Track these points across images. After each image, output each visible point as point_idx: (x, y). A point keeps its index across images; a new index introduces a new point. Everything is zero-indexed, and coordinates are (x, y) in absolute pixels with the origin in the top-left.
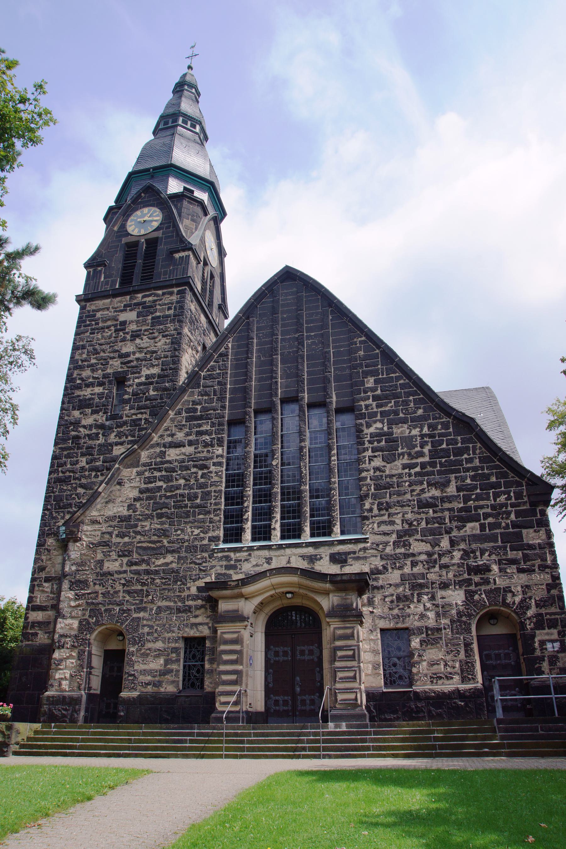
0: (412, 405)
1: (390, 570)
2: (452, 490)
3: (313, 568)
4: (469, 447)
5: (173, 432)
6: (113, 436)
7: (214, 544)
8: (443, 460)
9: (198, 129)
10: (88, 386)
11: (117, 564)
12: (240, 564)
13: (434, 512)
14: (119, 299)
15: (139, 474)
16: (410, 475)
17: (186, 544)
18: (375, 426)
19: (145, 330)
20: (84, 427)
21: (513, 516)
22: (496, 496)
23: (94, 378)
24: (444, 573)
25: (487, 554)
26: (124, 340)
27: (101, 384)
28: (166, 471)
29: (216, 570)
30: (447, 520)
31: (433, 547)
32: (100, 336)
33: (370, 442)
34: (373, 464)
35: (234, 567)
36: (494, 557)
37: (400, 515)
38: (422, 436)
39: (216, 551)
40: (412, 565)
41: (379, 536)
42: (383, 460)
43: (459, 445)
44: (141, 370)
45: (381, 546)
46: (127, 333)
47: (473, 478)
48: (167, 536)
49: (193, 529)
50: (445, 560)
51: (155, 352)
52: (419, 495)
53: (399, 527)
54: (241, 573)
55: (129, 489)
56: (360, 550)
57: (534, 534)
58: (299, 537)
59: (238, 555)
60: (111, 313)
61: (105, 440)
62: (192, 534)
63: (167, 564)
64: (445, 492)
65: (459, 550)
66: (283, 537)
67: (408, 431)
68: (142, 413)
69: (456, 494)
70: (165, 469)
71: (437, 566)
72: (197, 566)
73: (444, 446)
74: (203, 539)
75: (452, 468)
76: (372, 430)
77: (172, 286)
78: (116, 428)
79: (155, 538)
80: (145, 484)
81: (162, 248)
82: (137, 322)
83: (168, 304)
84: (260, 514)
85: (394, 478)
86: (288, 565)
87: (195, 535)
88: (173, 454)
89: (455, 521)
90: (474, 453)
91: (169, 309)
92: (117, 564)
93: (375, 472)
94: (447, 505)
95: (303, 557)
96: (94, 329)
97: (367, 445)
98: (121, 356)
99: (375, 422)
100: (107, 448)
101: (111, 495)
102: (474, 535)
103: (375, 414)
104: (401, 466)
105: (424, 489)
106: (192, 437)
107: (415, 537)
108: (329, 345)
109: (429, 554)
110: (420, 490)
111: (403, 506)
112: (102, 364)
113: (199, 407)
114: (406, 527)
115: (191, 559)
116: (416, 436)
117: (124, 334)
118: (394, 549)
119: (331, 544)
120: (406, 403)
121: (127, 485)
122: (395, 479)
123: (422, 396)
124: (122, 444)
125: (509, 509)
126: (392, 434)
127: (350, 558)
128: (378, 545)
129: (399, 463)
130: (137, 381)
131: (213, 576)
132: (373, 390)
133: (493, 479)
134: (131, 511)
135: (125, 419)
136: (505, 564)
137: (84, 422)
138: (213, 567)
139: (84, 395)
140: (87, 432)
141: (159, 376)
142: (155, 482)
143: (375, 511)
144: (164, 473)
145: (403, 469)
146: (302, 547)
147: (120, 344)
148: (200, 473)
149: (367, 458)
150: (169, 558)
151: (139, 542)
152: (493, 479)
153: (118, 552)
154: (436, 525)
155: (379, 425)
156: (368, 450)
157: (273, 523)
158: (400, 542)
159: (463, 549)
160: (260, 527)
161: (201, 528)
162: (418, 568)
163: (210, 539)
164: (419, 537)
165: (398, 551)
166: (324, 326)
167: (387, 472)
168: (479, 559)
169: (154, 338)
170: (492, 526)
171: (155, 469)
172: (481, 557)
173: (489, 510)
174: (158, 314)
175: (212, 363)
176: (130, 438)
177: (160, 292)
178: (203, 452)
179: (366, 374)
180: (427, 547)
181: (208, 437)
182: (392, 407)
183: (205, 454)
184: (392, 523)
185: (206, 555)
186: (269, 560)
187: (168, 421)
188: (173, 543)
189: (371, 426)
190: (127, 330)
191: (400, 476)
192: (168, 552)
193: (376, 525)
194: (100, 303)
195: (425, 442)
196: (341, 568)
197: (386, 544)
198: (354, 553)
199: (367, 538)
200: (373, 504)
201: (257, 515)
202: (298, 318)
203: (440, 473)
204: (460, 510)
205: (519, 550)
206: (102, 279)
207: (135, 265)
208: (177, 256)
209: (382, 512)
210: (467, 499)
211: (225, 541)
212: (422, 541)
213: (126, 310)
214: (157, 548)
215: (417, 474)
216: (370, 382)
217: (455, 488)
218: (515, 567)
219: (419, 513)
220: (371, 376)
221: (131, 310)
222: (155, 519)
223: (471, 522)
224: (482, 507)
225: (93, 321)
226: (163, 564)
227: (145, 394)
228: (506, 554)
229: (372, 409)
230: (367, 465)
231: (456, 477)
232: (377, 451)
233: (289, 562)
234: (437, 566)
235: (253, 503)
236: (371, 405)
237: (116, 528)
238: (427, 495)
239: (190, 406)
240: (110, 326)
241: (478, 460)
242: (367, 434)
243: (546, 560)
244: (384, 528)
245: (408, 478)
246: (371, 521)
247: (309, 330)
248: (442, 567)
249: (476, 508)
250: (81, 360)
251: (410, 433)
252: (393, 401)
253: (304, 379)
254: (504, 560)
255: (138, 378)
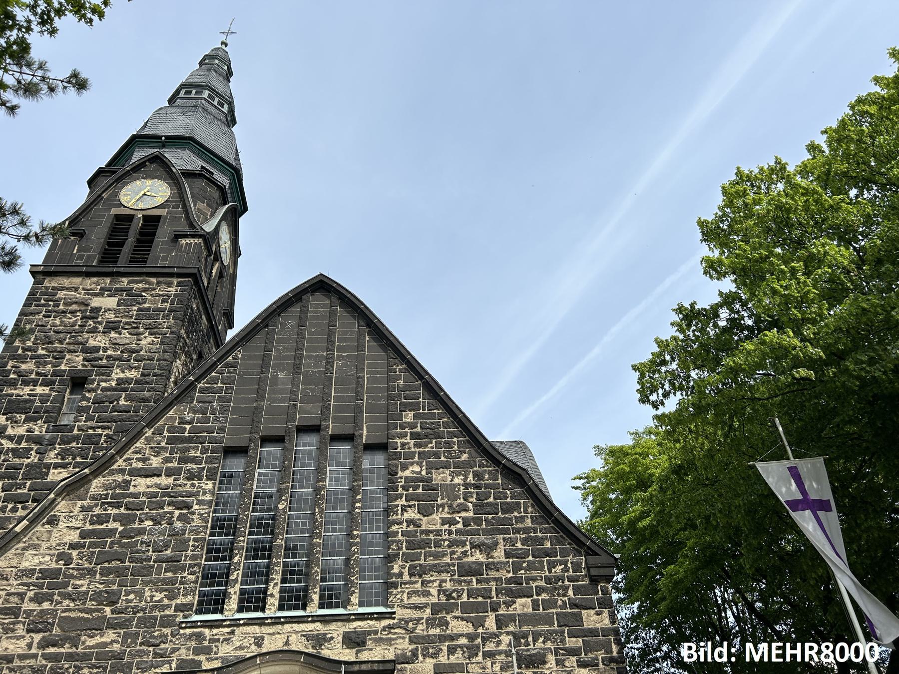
0: (456, 447)
1: (421, 658)
2: (499, 554)
3: (320, 653)
4: (520, 503)
5: (147, 456)
6: (52, 454)
7: (182, 614)
8: (490, 516)
9: (225, 109)
10: (26, 383)
11: (23, 643)
12: (216, 646)
13: (478, 581)
14: (95, 279)
15: (83, 509)
16: (450, 533)
17: (140, 614)
18: (411, 469)
19: (127, 323)
20: (10, 438)
21: (570, 592)
22: (551, 565)
23: (38, 374)
24: (489, 664)
25: (541, 640)
26: (94, 331)
27: (45, 384)
28: (127, 509)
29: (180, 655)
30: (494, 593)
31: (476, 627)
32: (57, 322)
33: (405, 488)
34: (406, 515)
35: (207, 651)
36: (549, 645)
37: (436, 584)
38: (466, 486)
39: (184, 625)
40: (448, 651)
41: (408, 611)
42: (418, 512)
43: (509, 500)
44: (112, 371)
45: (410, 625)
46: (100, 323)
47: (524, 542)
48: (112, 603)
49: (155, 593)
50: (490, 646)
51: (138, 351)
52: (459, 558)
53: (435, 600)
54: (216, 659)
55: (65, 531)
56: (384, 629)
57: (595, 617)
58: (304, 608)
59: (215, 631)
60: (80, 296)
61: (39, 460)
62: (151, 599)
63: (105, 645)
64: (492, 557)
65: (508, 633)
66: (281, 608)
67: (450, 478)
68: (103, 428)
69: (505, 560)
70: (126, 505)
71: (480, 654)
72: (151, 649)
73: (491, 500)
74: (169, 606)
75: (501, 527)
76: (407, 473)
77: (172, 275)
78: (59, 444)
79: (89, 604)
80: (92, 523)
81: (164, 232)
82: (116, 312)
83: (163, 295)
84: (253, 574)
85: (431, 535)
86: (285, 648)
87: (156, 601)
88: (141, 485)
89: (502, 594)
90: (526, 511)
91: (163, 301)
92: (23, 643)
93: (408, 526)
94: (493, 574)
95: (308, 637)
96: (50, 311)
97: (400, 491)
98: (86, 350)
99: (412, 464)
100: (39, 471)
101: (34, 538)
102: (525, 615)
103: (411, 455)
104: (439, 521)
105: (467, 551)
106: (174, 465)
107: (454, 614)
108: (364, 369)
109: (471, 637)
110: (462, 552)
111: (440, 572)
112: (54, 358)
113: (188, 427)
114: (443, 599)
115: (144, 637)
116: (459, 484)
117: (94, 323)
118: (427, 628)
119: (346, 619)
120: (449, 444)
121: (62, 525)
122: (431, 536)
123: (467, 438)
124: (64, 466)
125: (567, 583)
126: (431, 480)
127: (370, 639)
128: (407, 622)
129: (437, 517)
130: (103, 384)
131: (174, 665)
132: (412, 426)
133: (548, 545)
134: (62, 562)
135: (75, 432)
136: (563, 655)
137: (10, 431)
138: (174, 650)
139: (18, 395)
140: (11, 446)
141: (137, 382)
142: (108, 522)
143: (406, 577)
144: (122, 510)
145: (443, 524)
146: (307, 622)
147: (86, 335)
148: (177, 513)
149: (399, 508)
150: (110, 635)
151: (63, 611)
152: (548, 545)
153: (28, 624)
154: (480, 599)
155: (417, 468)
156: (401, 498)
157: (270, 588)
158: (435, 619)
159: (512, 632)
160: (252, 592)
161: (166, 590)
162: (456, 655)
163: (178, 608)
164: (458, 613)
165: (432, 632)
166: (360, 347)
167: (423, 527)
168: (532, 647)
169: (138, 334)
170: (548, 604)
171: (109, 504)
172: (534, 644)
173: (543, 583)
174: (147, 305)
175: (213, 374)
176: (78, 460)
177: (154, 280)
178: (185, 485)
179: (405, 407)
180: (468, 628)
181: (194, 466)
182: (432, 448)
183: (187, 488)
184: (427, 594)
185: (167, 631)
186: (259, 641)
187: (142, 440)
188: (119, 613)
189: (407, 469)
190: (100, 319)
191: (438, 533)
192: (112, 626)
193: (405, 595)
194: (66, 282)
195: (469, 492)
196: (357, 654)
197: (418, 621)
198: (376, 632)
199: (394, 613)
200: (403, 567)
201: (250, 574)
202: (330, 334)
203: (486, 532)
204: (509, 581)
205: (579, 637)
206: (75, 251)
207: (124, 243)
208: (183, 241)
209: (413, 579)
210: (516, 568)
211: (199, 612)
212: (463, 619)
213: (102, 295)
214: (93, 619)
215: (458, 532)
216: (409, 417)
217: (503, 551)
218: (574, 659)
219: (460, 582)
220: (410, 410)
221: (109, 296)
222: (98, 576)
223: (521, 597)
224: (535, 579)
225: (51, 301)
226: (98, 646)
227: (112, 402)
228: (563, 641)
229: (409, 448)
230: (399, 516)
231: (504, 539)
232: (412, 500)
233: (287, 643)
234: (480, 654)
235: (245, 559)
236: (409, 443)
237: (31, 588)
238: (470, 559)
239: (176, 424)
240: (76, 311)
241: (530, 520)
242: (401, 478)
243: (612, 653)
244: (415, 600)
245: (447, 536)
246: (399, 590)
247: (340, 349)
248: (487, 655)
249: (528, 580)
250: (23, 348)
251: (452, 480)
252: (434, 441)
253: (330, 405)
254: (561, 649)
255: (106, 381)
